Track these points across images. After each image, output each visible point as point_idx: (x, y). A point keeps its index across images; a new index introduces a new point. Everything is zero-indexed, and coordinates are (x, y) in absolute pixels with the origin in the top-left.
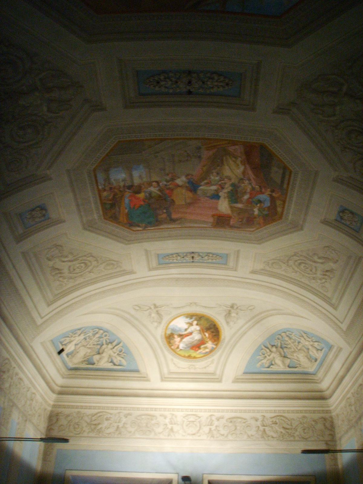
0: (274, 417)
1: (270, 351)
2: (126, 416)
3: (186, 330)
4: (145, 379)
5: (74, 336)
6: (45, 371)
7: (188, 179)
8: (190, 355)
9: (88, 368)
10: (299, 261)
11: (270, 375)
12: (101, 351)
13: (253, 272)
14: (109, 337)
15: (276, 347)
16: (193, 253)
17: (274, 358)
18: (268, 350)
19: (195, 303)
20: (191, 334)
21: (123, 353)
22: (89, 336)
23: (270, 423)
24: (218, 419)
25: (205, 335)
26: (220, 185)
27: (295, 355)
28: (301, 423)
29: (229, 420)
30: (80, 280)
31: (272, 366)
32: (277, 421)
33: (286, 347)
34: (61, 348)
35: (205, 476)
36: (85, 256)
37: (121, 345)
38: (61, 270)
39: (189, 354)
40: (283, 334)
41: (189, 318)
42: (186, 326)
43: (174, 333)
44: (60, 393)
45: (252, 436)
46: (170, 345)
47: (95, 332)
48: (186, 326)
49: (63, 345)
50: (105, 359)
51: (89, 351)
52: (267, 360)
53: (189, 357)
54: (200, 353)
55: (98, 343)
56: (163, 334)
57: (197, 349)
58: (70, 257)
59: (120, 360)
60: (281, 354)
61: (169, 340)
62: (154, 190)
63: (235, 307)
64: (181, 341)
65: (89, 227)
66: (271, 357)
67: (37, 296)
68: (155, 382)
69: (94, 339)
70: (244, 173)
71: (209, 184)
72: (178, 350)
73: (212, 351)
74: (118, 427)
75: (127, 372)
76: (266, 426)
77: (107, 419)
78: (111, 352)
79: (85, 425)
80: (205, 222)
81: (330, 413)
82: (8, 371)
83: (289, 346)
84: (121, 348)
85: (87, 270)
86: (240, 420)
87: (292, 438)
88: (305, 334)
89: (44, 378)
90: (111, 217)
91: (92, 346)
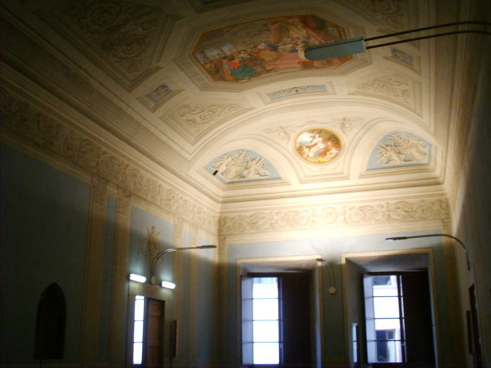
0: (397, 203)
1: (386, 150)
2: (277, 214)
3: (311, 142)
4: (287, 183)
5: (222, 160)
6: (206, 190)
7: (267, 44)
8: (319, 161)
9: (240, 181)
10: (381, 84)
11: (390, 169)
12: (248, 166)
13: (350, 94)
14: (252, 155)
15: (391, 146)
16: (295, 88)
17: (391, 155)
18: (384, 150)
19: (313, 121)
20: (316, 144)
21: (265, 166)
22: (236, 158)
23: (394, 208)
24: (350, 209)
25: (328, 144)
26: (294, 43)
27: (408, 150)
28: (420, 206)
29: (359, 209)
30: (212, 123)
31: (389, 162)
32: (400, 206)
33: (399, 146)
34: (215, 170)
35: (342, 254)
36: (210, 106)
37: (262, 160)
38: (194, 120)
39: (319, 160)
40: (393, 135)
41: (311, 133)
42: (311, 139)
43: (302, 145)
44: (224, 202)
45: (379, 220)
46: (301, 155)
47: (240, 154)
48: (311, 139)
49: (215, 168)
50: (253, 173)
51: (239, 168)
52: (385, 158)
53: (319, 162)
54: (327, 158)
55: (244, 160)
56: (294, 147)
57: (324, 155)
58: (198, 110)
59: (265, 172)
60: (395, 151)
61: (300, 151)
62: (243, 55)
63: (347, 120)
64: (309, 151)
65: (205, 88)
66: (388, 154)
67: (182, 142)
68: (295, 186)
69: (240, 158)
70: (307, 33)
71: (284, 44)
72: (309, 158)
73: (336, 155)
74: (272, 223)
75: (272, 180)
76: (391, 211)
77: (263, 218)
78: (256, 166)
79: (246, 224)
80: (293, 68)
81: (446, 195)
82: (173, 198)
83: (401, 144)
84: (263, 162)
85: (215, 115)
86: (368, 208)
87: (412, 219)
88: (409, 135)
89: (206, 194)
90: (219, 78)
91: (240, 164)
